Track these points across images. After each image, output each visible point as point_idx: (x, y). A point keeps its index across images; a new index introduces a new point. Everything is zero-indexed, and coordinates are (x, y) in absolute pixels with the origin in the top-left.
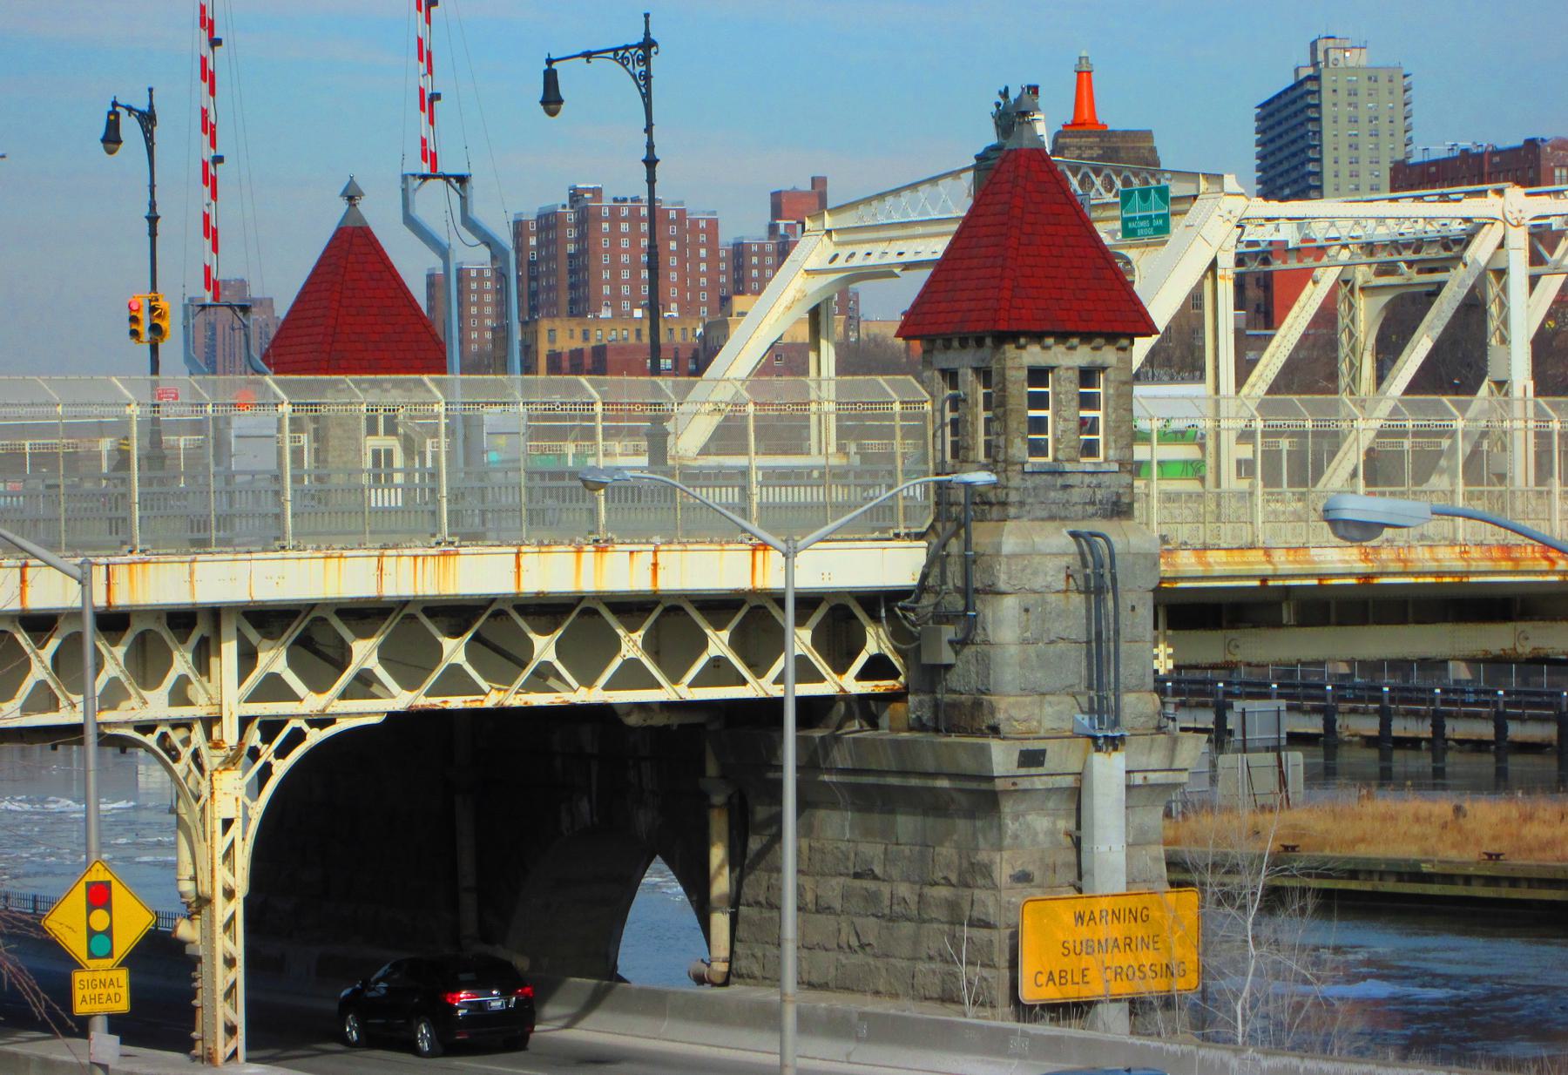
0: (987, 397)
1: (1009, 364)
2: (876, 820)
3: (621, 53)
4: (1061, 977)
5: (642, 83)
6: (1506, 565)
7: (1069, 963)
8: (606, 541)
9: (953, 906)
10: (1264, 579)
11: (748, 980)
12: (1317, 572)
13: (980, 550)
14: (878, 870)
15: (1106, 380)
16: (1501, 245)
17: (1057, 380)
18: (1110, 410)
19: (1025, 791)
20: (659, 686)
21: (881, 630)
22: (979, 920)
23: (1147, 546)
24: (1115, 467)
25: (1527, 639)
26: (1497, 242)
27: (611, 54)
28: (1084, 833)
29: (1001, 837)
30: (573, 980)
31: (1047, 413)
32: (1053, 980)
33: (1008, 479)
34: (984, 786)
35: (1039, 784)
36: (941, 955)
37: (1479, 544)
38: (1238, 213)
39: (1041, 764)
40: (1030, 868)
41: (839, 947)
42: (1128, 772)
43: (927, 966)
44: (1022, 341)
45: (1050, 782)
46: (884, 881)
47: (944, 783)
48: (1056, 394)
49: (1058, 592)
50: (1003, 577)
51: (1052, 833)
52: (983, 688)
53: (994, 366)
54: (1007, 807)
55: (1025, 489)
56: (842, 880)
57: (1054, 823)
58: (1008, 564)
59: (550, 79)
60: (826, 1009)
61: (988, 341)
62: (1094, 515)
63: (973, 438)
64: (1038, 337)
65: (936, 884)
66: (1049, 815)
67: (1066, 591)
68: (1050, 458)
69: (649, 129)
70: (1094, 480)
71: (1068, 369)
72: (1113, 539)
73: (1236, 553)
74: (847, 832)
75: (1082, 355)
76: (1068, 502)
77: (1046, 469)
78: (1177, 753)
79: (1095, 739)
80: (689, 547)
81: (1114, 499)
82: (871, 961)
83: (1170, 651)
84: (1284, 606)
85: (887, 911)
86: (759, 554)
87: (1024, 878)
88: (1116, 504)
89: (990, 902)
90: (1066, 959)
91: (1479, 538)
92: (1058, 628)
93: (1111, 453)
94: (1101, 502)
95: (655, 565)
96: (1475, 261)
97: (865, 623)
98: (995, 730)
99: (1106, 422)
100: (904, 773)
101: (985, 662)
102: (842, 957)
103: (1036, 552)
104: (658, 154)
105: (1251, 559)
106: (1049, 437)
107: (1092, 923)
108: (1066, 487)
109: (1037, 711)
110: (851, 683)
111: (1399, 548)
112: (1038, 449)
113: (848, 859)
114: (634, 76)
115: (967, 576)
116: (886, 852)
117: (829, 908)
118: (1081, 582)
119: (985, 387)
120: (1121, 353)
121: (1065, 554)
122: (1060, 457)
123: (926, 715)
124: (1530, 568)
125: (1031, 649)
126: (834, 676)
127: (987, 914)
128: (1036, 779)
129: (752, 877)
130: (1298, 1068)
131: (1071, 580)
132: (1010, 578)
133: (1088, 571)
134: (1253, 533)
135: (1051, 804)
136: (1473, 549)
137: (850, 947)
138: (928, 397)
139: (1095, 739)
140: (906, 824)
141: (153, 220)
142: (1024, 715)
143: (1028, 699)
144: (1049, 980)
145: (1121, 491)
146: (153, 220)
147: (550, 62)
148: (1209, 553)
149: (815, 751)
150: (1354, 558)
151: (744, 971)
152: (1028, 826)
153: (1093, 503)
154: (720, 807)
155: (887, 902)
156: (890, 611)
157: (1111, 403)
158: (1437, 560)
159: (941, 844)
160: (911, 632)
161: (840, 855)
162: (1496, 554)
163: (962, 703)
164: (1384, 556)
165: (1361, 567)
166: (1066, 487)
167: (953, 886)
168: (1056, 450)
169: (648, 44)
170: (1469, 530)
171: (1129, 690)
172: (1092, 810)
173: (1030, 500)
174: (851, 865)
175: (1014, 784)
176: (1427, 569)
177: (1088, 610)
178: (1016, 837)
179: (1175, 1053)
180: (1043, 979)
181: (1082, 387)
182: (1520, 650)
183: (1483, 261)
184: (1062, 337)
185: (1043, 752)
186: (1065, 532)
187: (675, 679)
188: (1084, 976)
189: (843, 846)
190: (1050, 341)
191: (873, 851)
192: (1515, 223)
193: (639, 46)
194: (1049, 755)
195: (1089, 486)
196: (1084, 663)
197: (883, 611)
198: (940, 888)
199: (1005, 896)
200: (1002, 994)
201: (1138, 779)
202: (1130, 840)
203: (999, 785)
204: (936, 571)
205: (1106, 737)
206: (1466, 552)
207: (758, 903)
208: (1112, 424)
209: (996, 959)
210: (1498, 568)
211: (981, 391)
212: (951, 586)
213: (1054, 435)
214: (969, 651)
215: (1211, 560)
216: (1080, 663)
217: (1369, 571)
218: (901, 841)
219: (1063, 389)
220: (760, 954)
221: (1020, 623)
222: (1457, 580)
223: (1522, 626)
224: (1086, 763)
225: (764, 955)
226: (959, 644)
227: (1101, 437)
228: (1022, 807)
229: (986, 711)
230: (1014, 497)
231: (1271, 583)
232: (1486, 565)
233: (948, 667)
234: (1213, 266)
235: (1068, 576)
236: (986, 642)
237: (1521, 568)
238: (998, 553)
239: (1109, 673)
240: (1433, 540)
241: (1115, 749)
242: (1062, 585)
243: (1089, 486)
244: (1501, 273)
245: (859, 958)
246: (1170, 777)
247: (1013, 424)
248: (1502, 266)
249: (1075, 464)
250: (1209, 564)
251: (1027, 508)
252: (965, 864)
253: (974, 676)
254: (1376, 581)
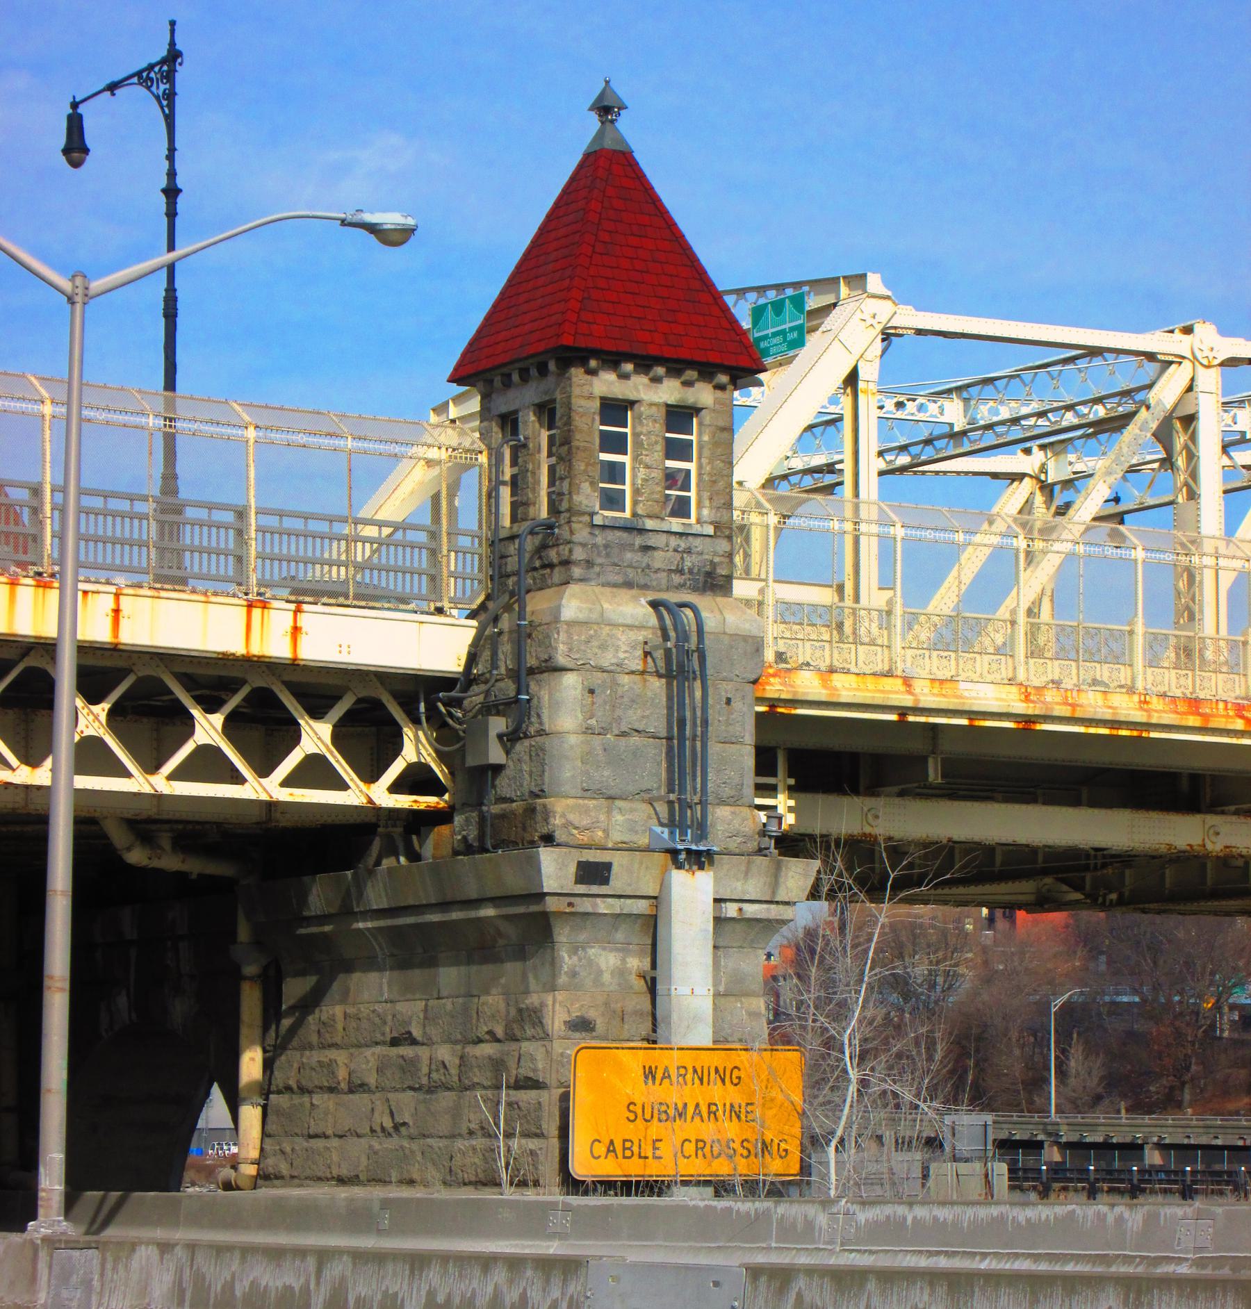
0: (551, 439)
1: (576, 391)
2: (417, 975)
3: (145, 74)
4: (625, 1149)
5: (165, 103)
6: (1193, 721)
7: (632, 1131)
8: (53, 575)
9: (498, 1065)
10: (903, 711)
11: (276, 1182)
12: (966, 708)
13: (537, 620)
14: (417, 1033)
15: (700, 424)
16: (1190, 389)
17: (638, 418)
18: (704, 461)
19: (586, 915)
20: (128, 775)
21: (421, 733)
22: (528, 1079)
23: (747, 626)
24: (710, 530)
25: (1218, 834)
26: (1184, 383)
27: (135, 80)
28: (659, 973)
29: (554, 976)
30: (89, 1193)
31: (626, 459)
32: (614, 1151)
33: (572, 532)
34: (534, 908)
35: (603, 907)
36: (482, 1128)
37: (1164, 695)
38: (883, 318)
39: (605, 881)
40: (592, 1014)
41: (373, 1131)
42: (716, 901)
43: (466, 1143)
44: (593, 363)
45: (616, 906)
46: (423, 1044)
47: (489, 912)
48: (636, 435)
49: (633, 672)
50: (562, 648)
51: (621, 972)
52: (536, 790)
53: (558, 396)
54: (562, 934)
55: (594, 545)
56: (378, 1050)
57: (623, 960)
58: (570, 636)
59: (75, 125)
60: (346, 1199)
61: (552, 366)
62: (682, 586)
63: (534, 490)
64: (612, 361)
65: (480, 1041)
66: (618, 950)
67: (643, 673)
68: (627, 514)
69: (171, 157)
70: (683, 544)
71: (651, 404)
72: (704, 614)
73: (870, 679)
74: (385, 988)
75: (669, 391)
76: (648, 566)
77: (622, 524)
78: (782, 880)
79: (674, 853)
80: (163, 594)
81: (708, 568)
82: (406, 1143)
83: (792, 803)
84: (931, 762)
85: (425, 1081)
86: (256, 612)
87: (582, 1025)
88: (709, 574)
89: (540, 1055)
90: (632, 1126)
91: (1162, 689)
92: (633, 717)
93: (705, 512)
94: (691, 571)
95: (117, 611)
96: (1159, 402)
97: (401, 723)
98: (549, 839)
99: (700, 475)
100: (444, 906)
101: (539, 756)
102: (376, 1145)
103: (604, 621)
104: (180, 182)
105: (888, 688)
106: (627, 488)
107: (666, 1081)
108: (646, 548)
109: (602, 817)
110: (381, 794)
111: (1067, 690)
112: (613, 500)
113: (385, 1023)
114: (157, 98)
115: (519, 654)
116: (426, 1010)
117: (362, 1085)
118: (661, 664)
119: (549, 429)
120: (719, 393)
121: (641, 627)
122: (640, 512)
123: (472, 834)
124: (1222, 726)
125: (597, 740)
126: (361, 784)
127: (535, 1070)
128: (599, 900)
129: (283, 1058)
130: (905, 1219)
131: (649, 659)
132: (570, 650)
133: (669, 644)
134: (891, 659)
135: (619, 936)
136: (1155, 699)
137: (383, 1129)
138: (483, 447)
139: (674, 853)
140: (449, 976)
141: (172, 192)
142: (585, 822)
143: (591, 803)
144: (609, 1151)
145: (717, 559)
146: (172, 192)
147: (75, 105)
148: (835, 676)
149: (348, 893)
150: (1011, 697)
151: (271, 1170)
152: (590, 962)
153: (680, 571)
154: (251, 979)
155: (425, 1070)
156: (432, 709)
157: (706, 452)
158: (1110, 707)
159: (488, 993)
160: (456, 731)
161: (377, 1020)
162: (1182, 707)
163: (513, 812)
164: (1049, 699)
165: (1020, 708)
166: (646, 548)
167: (498, 1041)
168: (635, 503)
169: (173, 56)
170: (1150, 679)
171: (722, 802)
172: (669, 951)
173: (599, 560)
174: (388, 1030)
175: (570, 904)
176: (1099, 717)
177: (670, 698)
178: (573, 974)
179: (748, 1213)
180: (601, 1149)
181: (668, 431)
182: (1210, 846)
183: (1169, 402)
184: (644, 364)
185: (608, 866)
186: (643, 601)
187: (152, 767)
188: (655, 1148)
189: (379, 1008)
190: (628, 367)
191: (412, 1009)
192: (1205, 362)
193: (163, 62)
194: (615, 869)
195: (675, 550)
196: (664, 765)
197: (422, 705)
198: (482, 1045)
199: (557, 1047)
200: (549, 1170)
201: (731, 910)
202: (722, 989)
203: (552, 904)
204: (486, 654)
205: (689, 851)
206: (1146, 702)
207: (288, 1089)
208: (706, 478)
209: (544, 1126)
210: (1184, 723)
211: (544, 435)
212: (503, 670)
213: (633, 484)
214: (521, 747)
215: (839, 685)
216: (659, 764)
217: (1030, 712)
218: (444, 993)
219: (644, 430)
220: (288, 1149)
221: (583, 706)
222: (1135, 733)
223: (1212, 819)
224: (664, 885)
225: (293, 1150)
226: (510, 739)
227: (693, 494)
228: (582, 937)
229: (539, 818)
230: (579, 554)
231: (911, 719)
232: (1168, 719)
233: (498, 769)
234: (852, 380)
235: (646, 654)
236: (541, 733)
237: (1211, 725)
238: (556, 619)
239: (694, 780)
240: (1107, 685)
241: (701, 868)
242: (637, 665)
243: (675, 550)
244: (1189, 420)
245: (392, 1143)
246: (773, 912)
247: (579, 466)
248: (1189, 411)
249: (658, 521)
250: (835, 689)
251: (597, 569)
252: (513, 1012)
253: (527, 776)
254: (1039, 727)
